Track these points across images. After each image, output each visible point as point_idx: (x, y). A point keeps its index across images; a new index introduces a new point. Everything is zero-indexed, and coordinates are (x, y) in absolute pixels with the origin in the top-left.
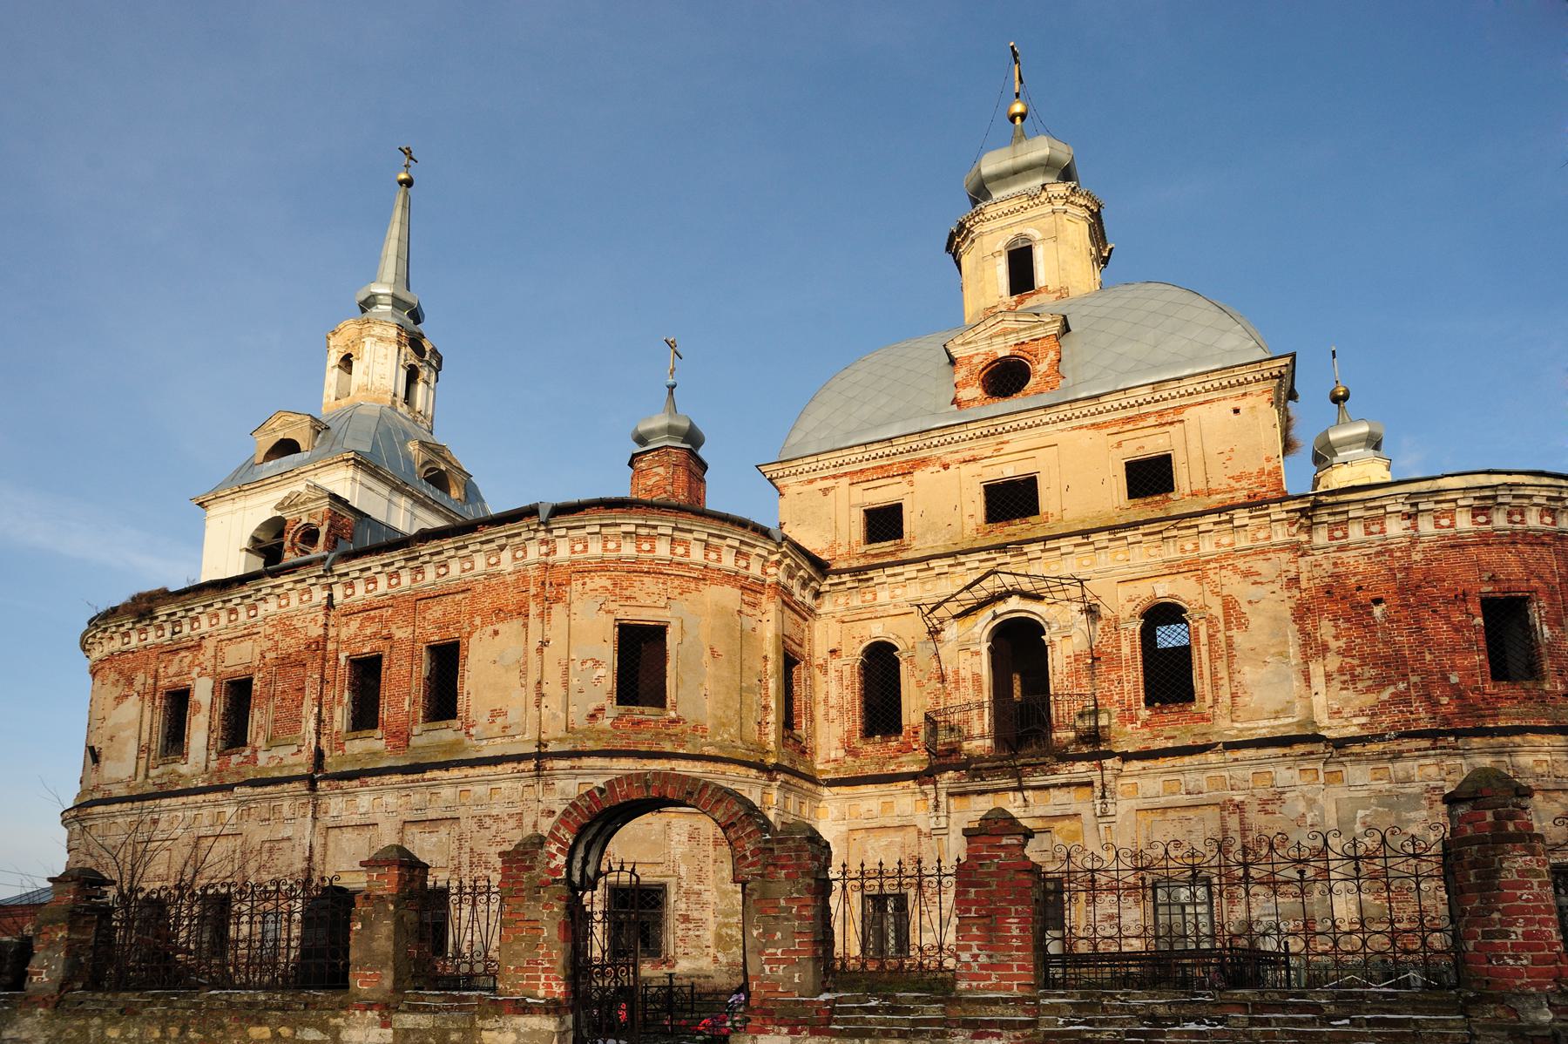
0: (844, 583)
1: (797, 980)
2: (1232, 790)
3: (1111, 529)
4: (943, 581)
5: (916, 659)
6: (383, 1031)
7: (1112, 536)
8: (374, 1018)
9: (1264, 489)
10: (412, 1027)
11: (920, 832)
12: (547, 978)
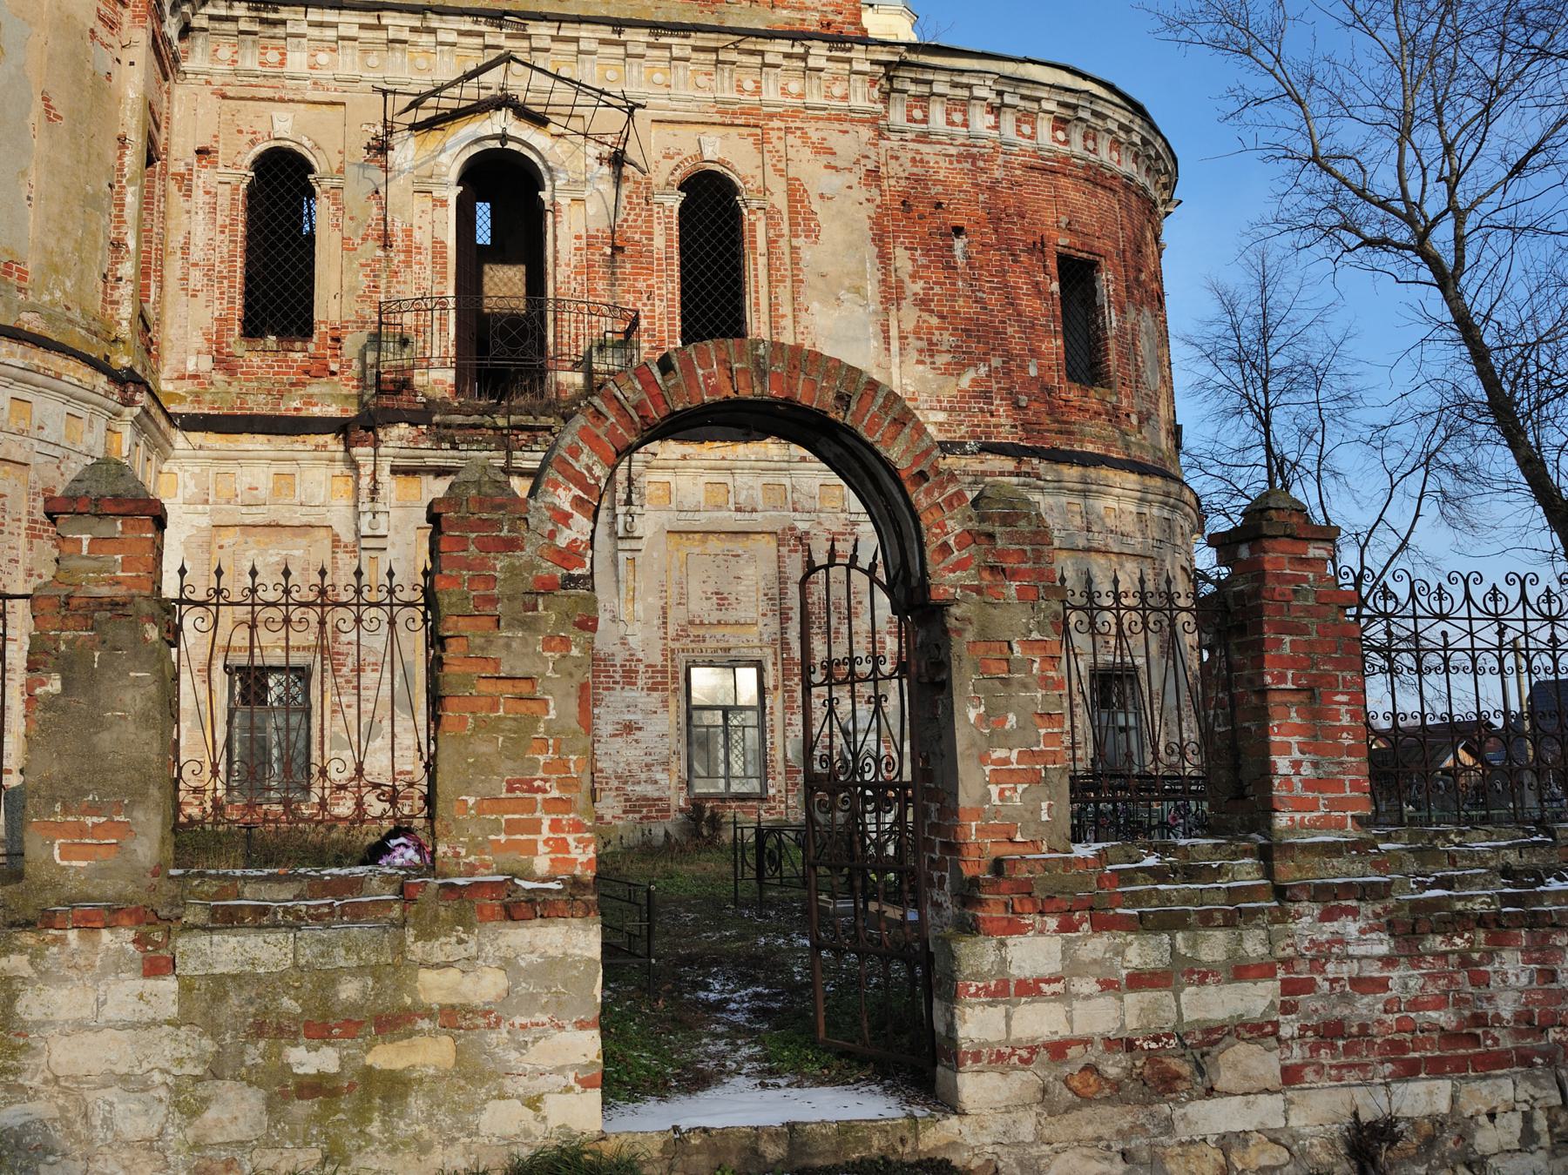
0: (235, 19)
1: (1045, 817)
2: (795, 510)
3: (655, 27)
4: (397, 56)
5: (346, 196)
6: (151, 984)
7: (652, 40)
8: (123, 951)
9: (839, 18)
10: (232, 969)
11: (336, 541)
12: (555, 826)
